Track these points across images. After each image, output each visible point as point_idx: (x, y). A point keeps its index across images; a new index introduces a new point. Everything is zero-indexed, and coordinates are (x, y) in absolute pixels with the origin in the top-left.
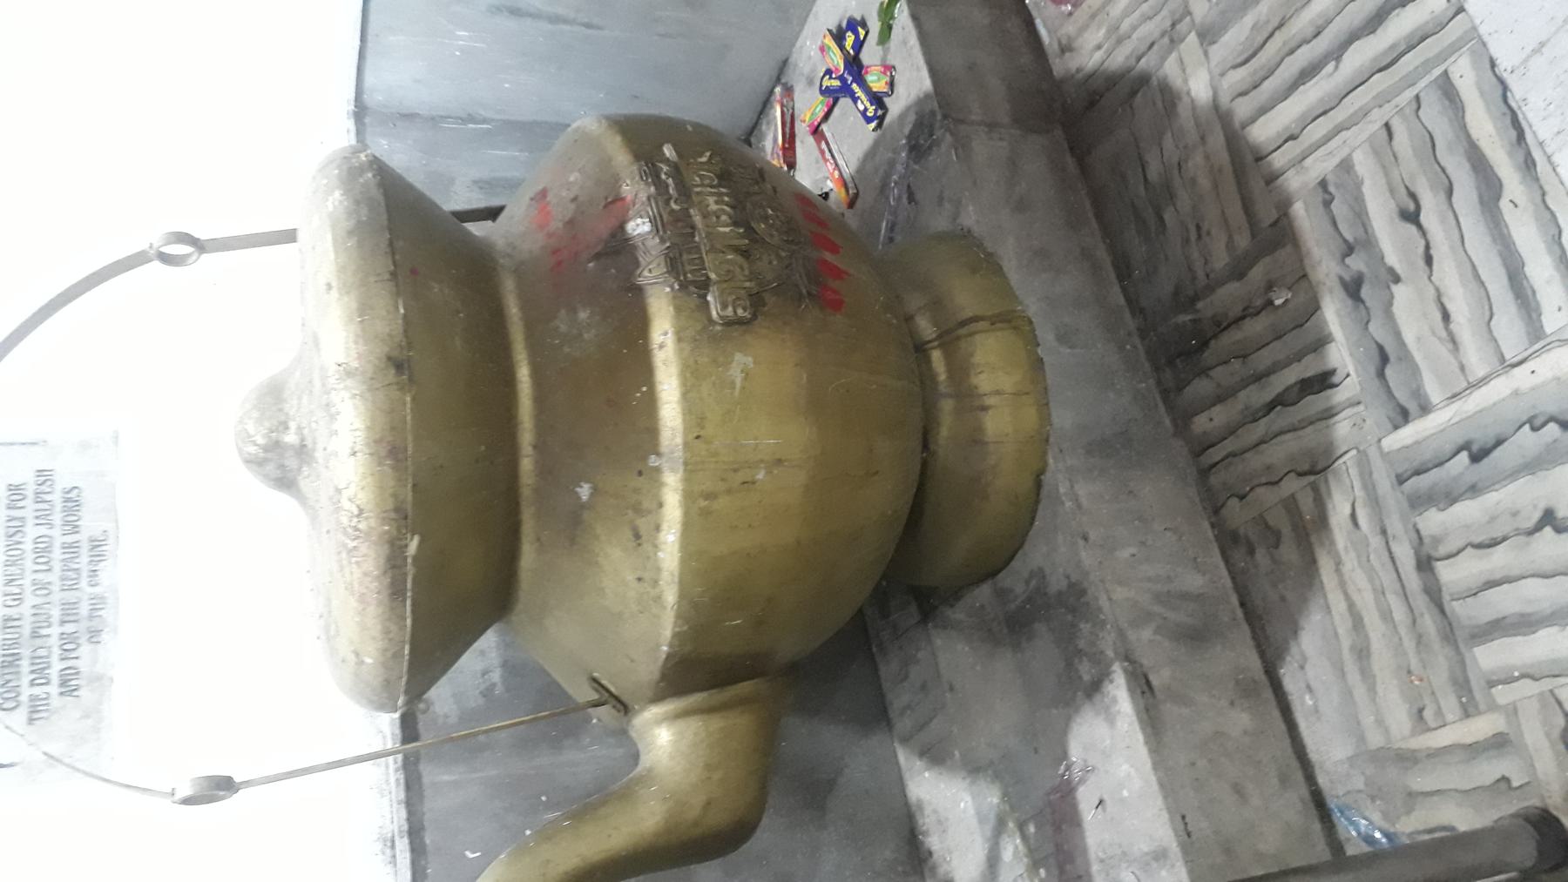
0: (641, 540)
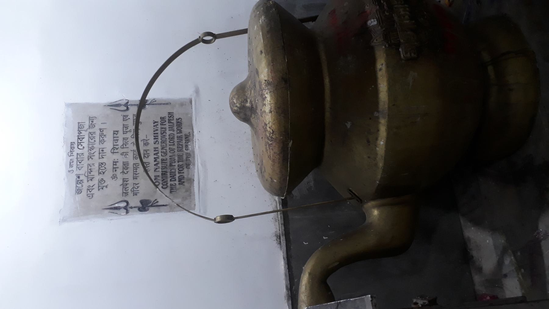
0: (371, 143)
